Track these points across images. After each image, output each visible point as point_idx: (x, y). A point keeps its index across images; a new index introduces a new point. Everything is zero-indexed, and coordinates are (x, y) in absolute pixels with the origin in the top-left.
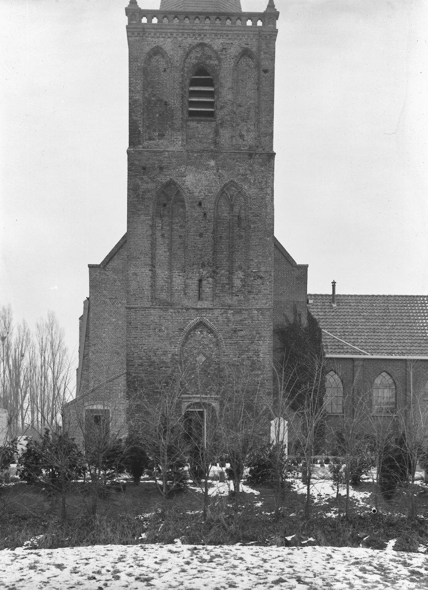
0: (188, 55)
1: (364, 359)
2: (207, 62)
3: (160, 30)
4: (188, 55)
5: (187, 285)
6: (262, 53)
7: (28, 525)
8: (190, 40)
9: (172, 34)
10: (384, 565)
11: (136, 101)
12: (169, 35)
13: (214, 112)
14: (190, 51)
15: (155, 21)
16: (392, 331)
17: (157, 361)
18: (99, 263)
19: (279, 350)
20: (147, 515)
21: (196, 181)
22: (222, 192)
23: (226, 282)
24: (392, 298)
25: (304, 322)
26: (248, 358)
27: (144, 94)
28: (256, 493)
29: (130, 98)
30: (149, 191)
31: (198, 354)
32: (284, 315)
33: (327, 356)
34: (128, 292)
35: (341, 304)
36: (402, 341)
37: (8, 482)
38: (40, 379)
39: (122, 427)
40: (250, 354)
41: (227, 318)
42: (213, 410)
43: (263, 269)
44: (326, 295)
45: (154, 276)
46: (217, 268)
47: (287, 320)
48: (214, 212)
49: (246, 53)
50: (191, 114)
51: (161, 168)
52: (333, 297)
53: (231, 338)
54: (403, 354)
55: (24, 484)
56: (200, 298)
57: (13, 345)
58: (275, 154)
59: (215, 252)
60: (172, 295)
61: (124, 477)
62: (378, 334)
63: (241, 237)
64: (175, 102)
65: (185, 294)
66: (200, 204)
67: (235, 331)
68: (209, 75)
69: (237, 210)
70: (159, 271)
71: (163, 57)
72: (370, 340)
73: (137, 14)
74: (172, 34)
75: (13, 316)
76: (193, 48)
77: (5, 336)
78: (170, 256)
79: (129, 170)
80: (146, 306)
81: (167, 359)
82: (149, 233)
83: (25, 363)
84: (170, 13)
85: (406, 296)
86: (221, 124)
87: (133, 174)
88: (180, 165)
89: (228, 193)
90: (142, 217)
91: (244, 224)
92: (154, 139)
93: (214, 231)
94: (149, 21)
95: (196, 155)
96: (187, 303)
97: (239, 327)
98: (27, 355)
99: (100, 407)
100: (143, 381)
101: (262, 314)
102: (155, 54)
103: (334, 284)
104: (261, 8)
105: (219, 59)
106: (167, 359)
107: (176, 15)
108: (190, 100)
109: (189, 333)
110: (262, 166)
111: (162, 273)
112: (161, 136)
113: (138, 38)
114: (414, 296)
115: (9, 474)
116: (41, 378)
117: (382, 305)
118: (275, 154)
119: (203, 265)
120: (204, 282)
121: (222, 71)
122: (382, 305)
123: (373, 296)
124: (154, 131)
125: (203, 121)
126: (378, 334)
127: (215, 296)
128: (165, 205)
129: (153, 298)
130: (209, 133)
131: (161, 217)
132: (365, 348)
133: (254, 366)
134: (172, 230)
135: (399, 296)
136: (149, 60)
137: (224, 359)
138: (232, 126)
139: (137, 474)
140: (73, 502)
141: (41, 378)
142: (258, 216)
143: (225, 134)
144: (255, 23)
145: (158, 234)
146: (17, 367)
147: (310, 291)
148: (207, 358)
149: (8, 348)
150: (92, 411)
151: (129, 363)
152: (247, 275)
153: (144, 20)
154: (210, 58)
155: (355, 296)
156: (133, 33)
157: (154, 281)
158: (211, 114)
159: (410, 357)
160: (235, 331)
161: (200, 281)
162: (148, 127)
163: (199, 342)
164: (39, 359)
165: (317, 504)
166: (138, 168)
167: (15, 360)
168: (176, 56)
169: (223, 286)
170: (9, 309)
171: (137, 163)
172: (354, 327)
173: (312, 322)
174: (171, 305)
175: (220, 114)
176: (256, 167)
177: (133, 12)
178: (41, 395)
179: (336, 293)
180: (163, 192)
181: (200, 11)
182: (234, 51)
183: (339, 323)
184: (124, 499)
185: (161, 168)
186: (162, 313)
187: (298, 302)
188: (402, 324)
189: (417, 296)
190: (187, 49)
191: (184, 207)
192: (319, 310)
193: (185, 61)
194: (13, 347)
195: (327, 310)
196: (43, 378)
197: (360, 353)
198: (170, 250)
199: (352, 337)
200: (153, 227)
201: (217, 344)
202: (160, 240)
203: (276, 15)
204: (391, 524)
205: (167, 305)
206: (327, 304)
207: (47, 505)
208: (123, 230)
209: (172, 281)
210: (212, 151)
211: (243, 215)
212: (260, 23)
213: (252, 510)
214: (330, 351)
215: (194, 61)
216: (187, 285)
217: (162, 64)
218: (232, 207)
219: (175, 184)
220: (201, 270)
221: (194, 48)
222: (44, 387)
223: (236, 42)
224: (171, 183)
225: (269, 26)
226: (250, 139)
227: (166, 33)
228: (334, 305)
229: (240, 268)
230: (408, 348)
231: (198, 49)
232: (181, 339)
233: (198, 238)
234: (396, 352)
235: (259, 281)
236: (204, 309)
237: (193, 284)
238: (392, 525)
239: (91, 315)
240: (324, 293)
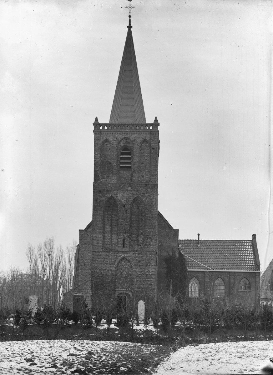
0: (119, 142)
1: (210, 272)
2: (128, 145)
3: (108, 132)
4: (119, 142)
5: (118, 242)
6: (152, 141)
7: (35, 338)
8: (120, 136)
9: (113, 134)
11: (97, 162)
12: (112, 134)
13: (131, 166)
14: (121, 141)
15: (106, 128)
16: (225, 258)
17: (105, 274)
18: (84, 229)
19: (165, 268)
20: (77, 335)
21: (122, 197)
22: (134, 201)
23: (135, 240)
24: (227, 242)
25: (177, 255)
26: (145, 273)
27: (100, 159)
28: (118, 328)
29: (94, 161)
30: (102, 201)
31: (123, 271)
32: (168, 252)
33: (189, 270)
34: (92, 245)
35: (202, 245)
36: (229, 263)
37: (31, 324)
38: (68, 276)
39: (267, 289)
40: (146, 271)
41: (135, 255)
42: (129, 295)
43: (152, 234)
44: (196, 240)
45: (104, 238)
46: (132, 234)
47: (169, 254)
48: (130, 210)
49: (145, 141)
50: (121, 167)
51: (108, 191)
52: (198, 241)
53: (137, 264)
54: (228, 269)
55: (36, 325)
56: (124, 247)
57: (54, 257)
59: (130, 227)
60: (112, 246)
61: (71, 323)
62: (218, 259)
63: (142, 220)
64: (114, 163)
65: (117, 245)
66: (124, 206)
67: (139, 261)
68: (129, 150)
69: (141, 209)
70: (106, 235)
71: (109, 143)
72: (214, 262)
73: (98, 126)
74: (113, 134)
75: (54, 243)
76: (122, 139)
77: (50, 253)
78: (111, 228)
79: (94, 192)
80: (100, 250)
81: (109, 273)
82: (102, 219)
83: (61, 267)
84: (113, 124)
85: (234, 241)
86: (134, 171)
87: (95, 193)
88: (116, 189)
89: (137, 201)
90: (99, 212)
91: (143, 215)
92: (105, 178)
93: (130, 218)
94: (103, 128)
95: (122, 185)
96: (118, 249)
97: (141, 260)
98: (61, 263)
99: (80, 295)
100: (100, 284)
101: (151, 254)
102: (105, 142)
103: (199, 235)
105: (133, 144)
106: (109, 273)
107: (115, 125)
108: (120, 161)
109: (119, 262)
110: (151, 189)
111: (108, 236)
112: (108, 177)
113: (98, 136)
114: (238, 241)
116: (69, 276)
117: (222, 245)
119: (125, 233)
120: (126, 240)
121: (134, 149)
122: (222, 245)
123: (218, 240)
124: (105, 175)
125: (126, 170)
126: (218, 259)
127: (130, 246)
128: (109, 207)
129: (103, 247)
130: (129, 175)
131: (108, 212)
132: (211, 266)
133: (147, 277)
134: (112, 217)
135: (231, 241)
136: (103, 145)
137: (134, 274)
138: (139, 172)
139: (76, 321)
140: (50, 330)
141: (69, 276)
142: (149, 211)
143: (136, 176)
144: (149, 128)
145: (106, 219)
146: (57, 269)
147: (180, 238)
148: (127, 273)
149: (52, 260)
150: (76, 296)
151: (93, 275)
152: (145, 237)
154: (129, 143)
155: (210, 240)
156: (96, 134)
157: (104, 240)
158: (130, 167)
159: (232, 271)
160: (139, 261)
161: (124, 240)
162: (102, 173)
163: (123, 266)
164: (68, 266)
165: (138, 332)
166: (97, 191)
167: (56, 266)
168: (115, 144)
169: (134, 241)
170: (53, 239)
171: (97, 189)
172: (207, 256)
173: (181, 255)
174: (111, 250)
175: (133, 167)
176: (149, 190)
177: (97, 124)
178: (69, 285)
179: (200, 239)
180: (108, 201)
181: (125, 123)
182: (140, 140)
183: (200, 254)
184: (71, 330)
185: (108, 191)
186: (107, 253)
187: (174, 246)
188: (230, 254)
189: (240, 241)
190: (119, 140)
191: (117, 207)
192: (191, 248)
193: (118, 146)
194: (54, 259)
195: (195, 248)
196: (70, 276)
197: (208, 269)
198: (111, 226)
199: (205, 261)
200: (104, 216)
201: (131, 267)
202: (107, 222)
203: (159, 125)
204: (162, 340)
205: (109, 250)
206: (195, 245)
207: (43, 332)
208: (91, 219)
209: (112, 240)
210: (130, 183)
211: (143, 211)
212: (151, 128)
213: (114, 334)
214: (193, 267)
215: (122, 145)
216: (118, 242)
217: (109, 146)
218: (138, 207)
219: (113, 198)
220: (124, 235)
221: (122, 139)
222: (70, 281)
223: (141, 136)
224: (111, 198)
225: (155, 129)
226: (146, 177)
227: (110, 133)
228: (199, 245)
229: (142, 234)
230: (231, 266)
231: (124, 140)
232: (115, 265)
233: (123, 221)
234: (225, 268)
235: (150, 240)
236: (126, 252)
237: (121, 241)
238: (162, 340)
239: (80, 252)
240: (195, 239)
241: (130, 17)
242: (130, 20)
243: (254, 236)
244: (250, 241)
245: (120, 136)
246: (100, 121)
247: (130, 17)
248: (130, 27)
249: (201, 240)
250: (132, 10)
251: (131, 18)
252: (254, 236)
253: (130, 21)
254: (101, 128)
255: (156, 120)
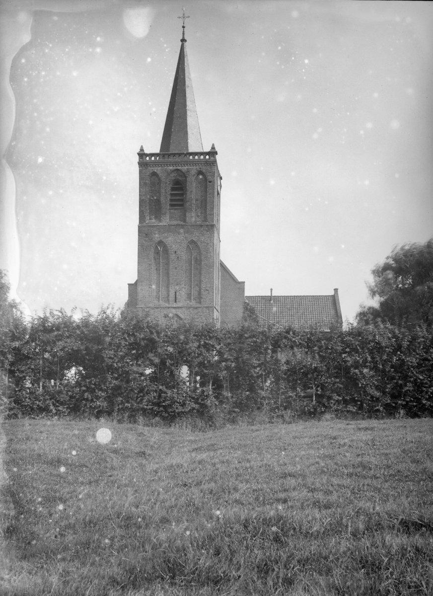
10: (172, 464)
44: (268, 296)
56: (176, 301)
58: (374, 272)
59: (174, 155)
66: (176, 252)
68: (181, 185)
104: (207, 149)
115: (75, 414)
118: (374, 272)
144: (205, 157)
147: (246, 295)
153: (148, 158)
177: (142, 155)
241: (184, 27)
242: (183, 32)
243: (336, 290)
244: (332, 296)
245: (171, 168)
246: (147, 151)
247: (184, 27)
248: (183, 40)
249: (274, 296)
250: (187, 20)
251: (185, 29)
252: (336, 290)
253: (183, 34)
254: (148, 158)
255: (213, 148)
